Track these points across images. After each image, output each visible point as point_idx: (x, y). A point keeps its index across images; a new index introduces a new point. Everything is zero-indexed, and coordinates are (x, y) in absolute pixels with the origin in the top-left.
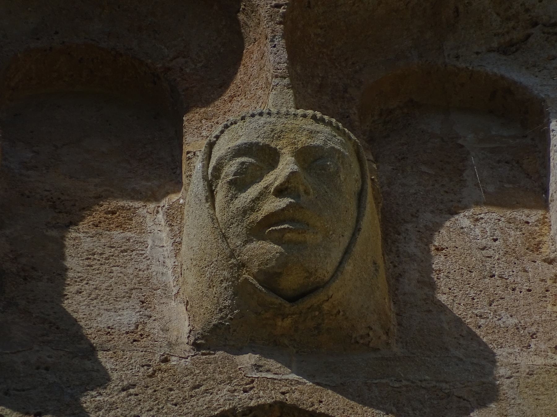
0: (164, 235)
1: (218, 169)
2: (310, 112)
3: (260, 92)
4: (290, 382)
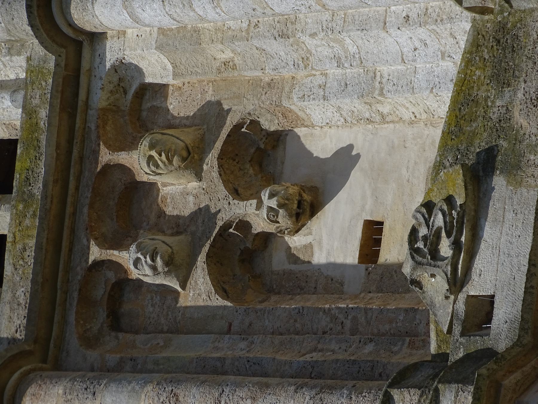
0: (169, 188)
1: (153, 172)
2: (139, 146)
3: (133, 160)
4: (212, 156)
